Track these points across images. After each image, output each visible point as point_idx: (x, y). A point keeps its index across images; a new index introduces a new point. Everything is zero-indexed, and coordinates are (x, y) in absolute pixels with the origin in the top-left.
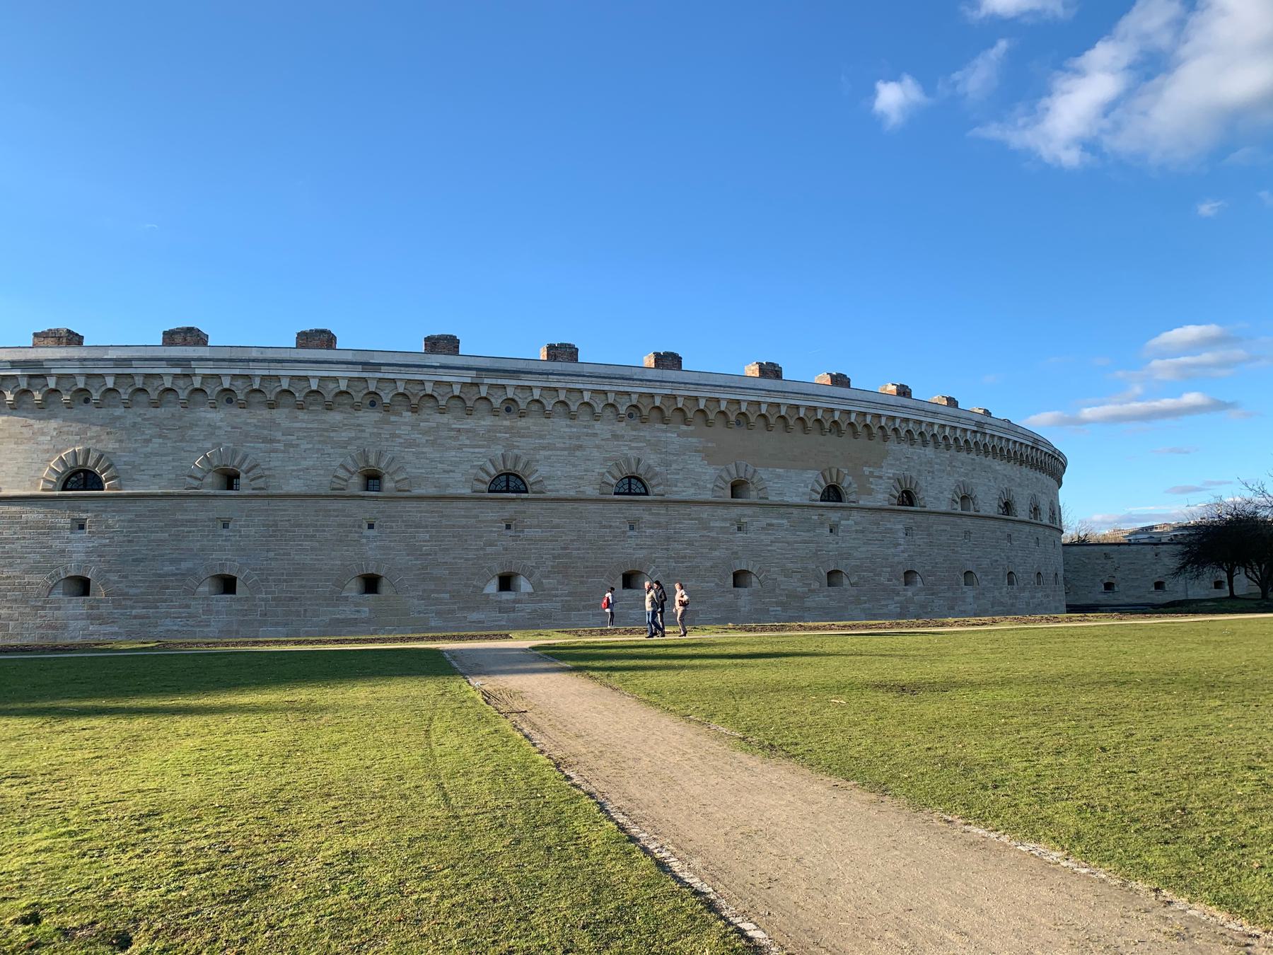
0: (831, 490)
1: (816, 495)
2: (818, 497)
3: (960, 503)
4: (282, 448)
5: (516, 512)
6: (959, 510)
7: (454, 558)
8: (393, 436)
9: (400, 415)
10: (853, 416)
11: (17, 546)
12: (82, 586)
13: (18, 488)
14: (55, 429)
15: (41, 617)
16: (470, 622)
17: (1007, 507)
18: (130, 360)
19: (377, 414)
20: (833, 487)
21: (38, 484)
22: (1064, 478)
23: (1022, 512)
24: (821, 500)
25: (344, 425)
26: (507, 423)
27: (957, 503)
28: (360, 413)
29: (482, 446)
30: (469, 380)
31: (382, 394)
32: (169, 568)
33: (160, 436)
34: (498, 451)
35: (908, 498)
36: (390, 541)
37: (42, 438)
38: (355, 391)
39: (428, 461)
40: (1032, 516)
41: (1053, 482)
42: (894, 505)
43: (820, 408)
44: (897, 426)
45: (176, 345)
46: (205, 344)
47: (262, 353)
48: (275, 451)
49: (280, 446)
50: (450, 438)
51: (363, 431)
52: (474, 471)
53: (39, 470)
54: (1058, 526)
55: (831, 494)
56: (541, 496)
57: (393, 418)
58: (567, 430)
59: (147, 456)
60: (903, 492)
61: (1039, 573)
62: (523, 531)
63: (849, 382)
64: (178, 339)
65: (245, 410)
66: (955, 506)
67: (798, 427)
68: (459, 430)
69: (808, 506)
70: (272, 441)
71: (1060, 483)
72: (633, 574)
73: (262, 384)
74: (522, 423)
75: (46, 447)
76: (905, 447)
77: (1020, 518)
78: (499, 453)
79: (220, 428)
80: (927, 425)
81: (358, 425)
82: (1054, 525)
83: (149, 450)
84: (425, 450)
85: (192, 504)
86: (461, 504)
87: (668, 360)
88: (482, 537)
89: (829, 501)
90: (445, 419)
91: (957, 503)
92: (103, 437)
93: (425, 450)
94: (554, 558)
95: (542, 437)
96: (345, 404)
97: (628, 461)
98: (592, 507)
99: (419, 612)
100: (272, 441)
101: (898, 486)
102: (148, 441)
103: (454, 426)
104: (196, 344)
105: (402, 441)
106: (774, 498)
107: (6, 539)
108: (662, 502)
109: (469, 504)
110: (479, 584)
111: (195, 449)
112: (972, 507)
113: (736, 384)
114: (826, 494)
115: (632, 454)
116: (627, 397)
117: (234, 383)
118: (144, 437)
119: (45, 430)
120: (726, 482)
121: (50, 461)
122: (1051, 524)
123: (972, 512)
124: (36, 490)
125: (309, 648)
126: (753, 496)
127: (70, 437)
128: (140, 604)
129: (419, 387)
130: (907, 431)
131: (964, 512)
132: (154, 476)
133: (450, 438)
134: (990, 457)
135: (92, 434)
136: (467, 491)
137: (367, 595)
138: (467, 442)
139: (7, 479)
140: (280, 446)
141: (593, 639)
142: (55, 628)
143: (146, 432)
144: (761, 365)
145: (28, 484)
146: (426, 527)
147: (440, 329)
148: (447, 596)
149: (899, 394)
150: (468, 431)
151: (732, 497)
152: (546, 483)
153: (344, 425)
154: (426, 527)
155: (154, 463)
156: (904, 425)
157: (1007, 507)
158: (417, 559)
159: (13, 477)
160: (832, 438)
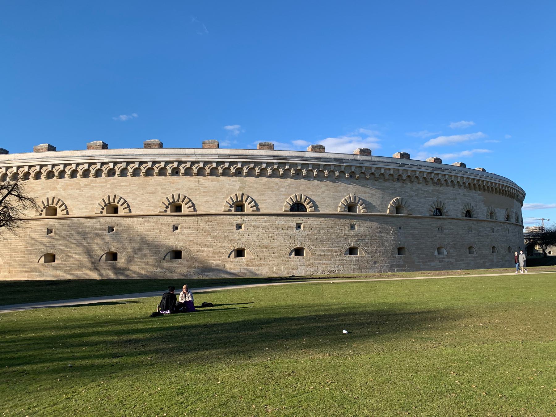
2: (464, 215)
5: (441, 223)
7: (426, 241)
8: (406, 192)
9: (407, 184)
10: (447, 177)
11: (275, 234)
12: (299, 252)
13: (273, 210)
14: (287, 185)
15: (287, 264)
16: (432, 266)
18: (286, 157)
19: (400, 184)
20: (437, 209)
21: (282, 209)
25: (390, 188)
26: (437, 188)
27: (488, 216)
28: (395, 183)
29: (430, 197)
30: (430, 171)
31: (403, 175)
32: (335, 244)
33: (328, 190)
34: (435, 199)
35: (469, 214)
36: (408, 234)
37: (282, 189)
38: (395, 174)
39: (416, 203)
40: (506, 219)
45: (316, 152)
46: (324, 152)
47: (362, 157)
50: (422, 194)
51: (396, 190)
52: (429, 207)
53: (282, 202)
54: (520, 224)
57: (405, 185)
58: (452, 192)
59: (324, 198)
60: (437, 209)
61: (519, 247)
62: (443, 231)
63: (370, 152)
64: (318, 150)
65: (357, 180)
68: (424, 191)
69: (504, 222)
72: (355, 248)
74: (441, 188)
75: (284, 193)
78: (436, 200)
81: (395, 188)
83: (324, 195)
84: (415, 198)
86: (426, 220)
87: (405, 156)
88: (432, 233)
90: (420, 186)
92: (306, 190)
93: (415, 198)
94: (452, 241)
95: (446, 194)
96: (390, 179)
97: (441, 202)
98: (460, 221)
99: (417, 262)
101: (465, 208)
103: (423, 189)
104: (320, 152)
105: (408, 194)
106: (262, 212)
107: (270, 231)
108: (476, 220)
109: (428, 220)
110: (433, 251)
111: (341, 195)
112: (494, 218)
113: (393, 161)
115: (468, 201)
118: (322, 190)
119: (283, 186)
121: (287, 199)
124: (281, 211)
127: (294, 189)
129: (414, 173)
130: (438, 179)
132: (327, 206)
133: (422, 194)
135: (302, 188)
136: (427, 215)
138: (427, 196)
139: (269, 206)
142: (293, 269)
143: (323, 188)
144: (401, 154)
145: (277, 208)
146: (417, 229)
148: (425, 256)
149: (483, 171)
150: (427, 191)
151: (349, 211)
152: (449, 212)
153: (390, 188)
154: (417, 229)
155: (326, 201)
158: (415, 242)
159: (271, 205)
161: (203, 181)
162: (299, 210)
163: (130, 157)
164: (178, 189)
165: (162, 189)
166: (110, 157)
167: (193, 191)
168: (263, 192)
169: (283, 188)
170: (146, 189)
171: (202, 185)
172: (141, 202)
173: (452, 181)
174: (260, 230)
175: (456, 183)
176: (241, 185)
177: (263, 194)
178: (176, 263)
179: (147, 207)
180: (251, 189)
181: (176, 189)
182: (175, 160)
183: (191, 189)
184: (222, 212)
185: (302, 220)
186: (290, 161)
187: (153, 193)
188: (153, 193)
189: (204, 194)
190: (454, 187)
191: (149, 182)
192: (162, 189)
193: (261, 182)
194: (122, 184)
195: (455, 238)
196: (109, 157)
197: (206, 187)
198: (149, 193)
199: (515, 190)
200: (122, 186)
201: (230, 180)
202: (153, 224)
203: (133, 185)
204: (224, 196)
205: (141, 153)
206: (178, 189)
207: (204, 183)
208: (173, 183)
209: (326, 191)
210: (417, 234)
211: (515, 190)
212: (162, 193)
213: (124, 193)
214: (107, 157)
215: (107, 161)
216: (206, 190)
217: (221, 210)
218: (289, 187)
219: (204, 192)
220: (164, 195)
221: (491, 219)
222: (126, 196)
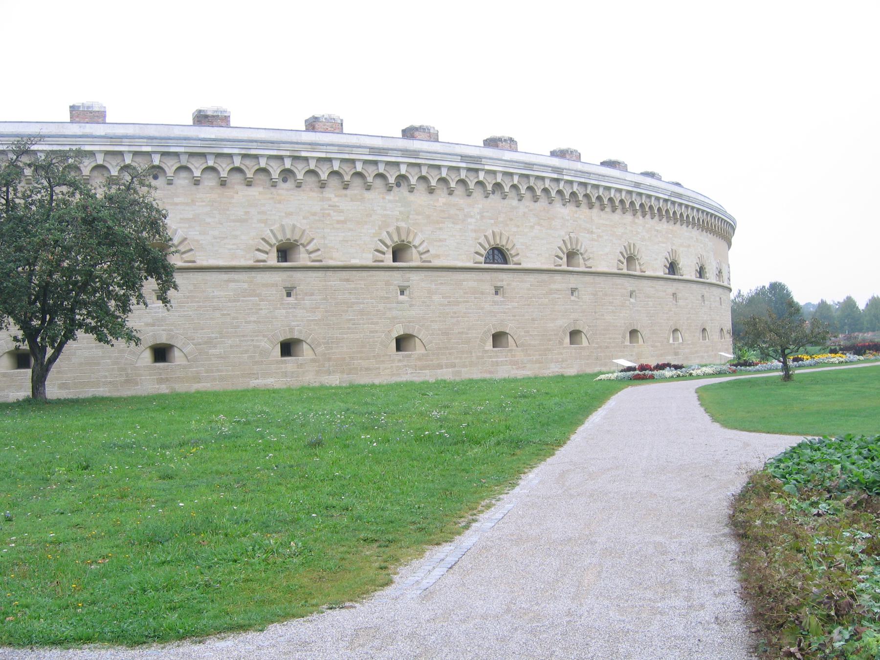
0: (496, 252)
1: (481, 257)
2: (482, 259)
3: (625, 263)
4: (596, 238)
6: (564, 267)
14: (478, 213)
17: (672, 267)
20: (493, 249)
22: (734, 240)
23: (688, 271)
24: (485, 263)
37: (469, 220)
40: (698, 275)
41: (725, 245)
42: (481, 263)
43: (516, 174)
44: (612, 196)
48: (593, 240)
49: (595, 236)
54: (725, 284)
55: (496, 257)
56: (381, 264)
66: (621, 266)
67: (528, 195)
70: (592, 233)
71: (729, 245)
73: (134, 160)
76: (570, 209)
77: (685, 277)
79: (568, 220)
80: (592, 187)
82: (721, 283)
85: (558, 277)
89: (493, 263)
91: (623, 263)
100: (592, 233)
102: (532, 227)
112: (638, 267)
114: (491, 257)
116: (349, 165)
117: (243, 162)
119: (472, 214)
120: (564, 254)
122: (718, 283)
123: (638, 273)
125: (747, 377)
126: (302, 258)
128: (537, 353)
130: (571, 193)
131: (571, 269)
132: (538, 255)
134: (672, 222)
137: (19, 370)
140: (595, 236)
141: (750, 376)
147: (209, 105)
151: (568, 266)
156: (607, 193)
157: (672, 267)
160: (496, 198)
161: (336, 199)
162: (496, 261)
163: (199, 143)
164: (289, 214)
165: (259, 213)
166: (155, 142)
167: (317, 218)
168: (441, 225)
169: (471, 217)
170: (228, 212)
171: (333, 206)
172: (218, 240)
173: (514, 187)
174: (436, 298)
175: (606, 201)
176: (402, 209)
177: (440, 229)
178: (501, 355)
179: (230, 249)
180: (420, 217)
181: (286, 213)
182: (182, 150)
183: (314, 214)
184: (370, 263)
185: (504, 279)
186: (487, 167)
187: (242, 221)
188: (242, 221)
189: (339, 226)
190: (578, 207)
191: (233, 198)
192: (259, 213)
193: (436, 204)
194: (176, 200)
195: (689, 313)
196: (154, 141)
197: (342, 211)
198: (234, 221)
199: (715, 218)
200: (177, 204)
201: (383, 198)
202: (246, 286)
203: (201, 204)
204: (374, 231)
205: (213, 137)
206: (289, 214)
207: (337, 204)
208: (280, 203)
209: (536, 227)
210: (652, 307)
211: (715, 218)
212: (260, 221)
213: (181, 219)
214: (150, 141)
215: (149, 149)
216: (342, 218)
217: (367, 260)
218: (482, 217)
219: (338, 222)
220: (263, 225)
221: (394, 260)
222: (187, 225)
